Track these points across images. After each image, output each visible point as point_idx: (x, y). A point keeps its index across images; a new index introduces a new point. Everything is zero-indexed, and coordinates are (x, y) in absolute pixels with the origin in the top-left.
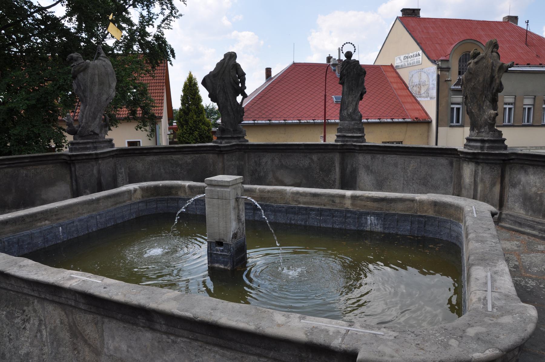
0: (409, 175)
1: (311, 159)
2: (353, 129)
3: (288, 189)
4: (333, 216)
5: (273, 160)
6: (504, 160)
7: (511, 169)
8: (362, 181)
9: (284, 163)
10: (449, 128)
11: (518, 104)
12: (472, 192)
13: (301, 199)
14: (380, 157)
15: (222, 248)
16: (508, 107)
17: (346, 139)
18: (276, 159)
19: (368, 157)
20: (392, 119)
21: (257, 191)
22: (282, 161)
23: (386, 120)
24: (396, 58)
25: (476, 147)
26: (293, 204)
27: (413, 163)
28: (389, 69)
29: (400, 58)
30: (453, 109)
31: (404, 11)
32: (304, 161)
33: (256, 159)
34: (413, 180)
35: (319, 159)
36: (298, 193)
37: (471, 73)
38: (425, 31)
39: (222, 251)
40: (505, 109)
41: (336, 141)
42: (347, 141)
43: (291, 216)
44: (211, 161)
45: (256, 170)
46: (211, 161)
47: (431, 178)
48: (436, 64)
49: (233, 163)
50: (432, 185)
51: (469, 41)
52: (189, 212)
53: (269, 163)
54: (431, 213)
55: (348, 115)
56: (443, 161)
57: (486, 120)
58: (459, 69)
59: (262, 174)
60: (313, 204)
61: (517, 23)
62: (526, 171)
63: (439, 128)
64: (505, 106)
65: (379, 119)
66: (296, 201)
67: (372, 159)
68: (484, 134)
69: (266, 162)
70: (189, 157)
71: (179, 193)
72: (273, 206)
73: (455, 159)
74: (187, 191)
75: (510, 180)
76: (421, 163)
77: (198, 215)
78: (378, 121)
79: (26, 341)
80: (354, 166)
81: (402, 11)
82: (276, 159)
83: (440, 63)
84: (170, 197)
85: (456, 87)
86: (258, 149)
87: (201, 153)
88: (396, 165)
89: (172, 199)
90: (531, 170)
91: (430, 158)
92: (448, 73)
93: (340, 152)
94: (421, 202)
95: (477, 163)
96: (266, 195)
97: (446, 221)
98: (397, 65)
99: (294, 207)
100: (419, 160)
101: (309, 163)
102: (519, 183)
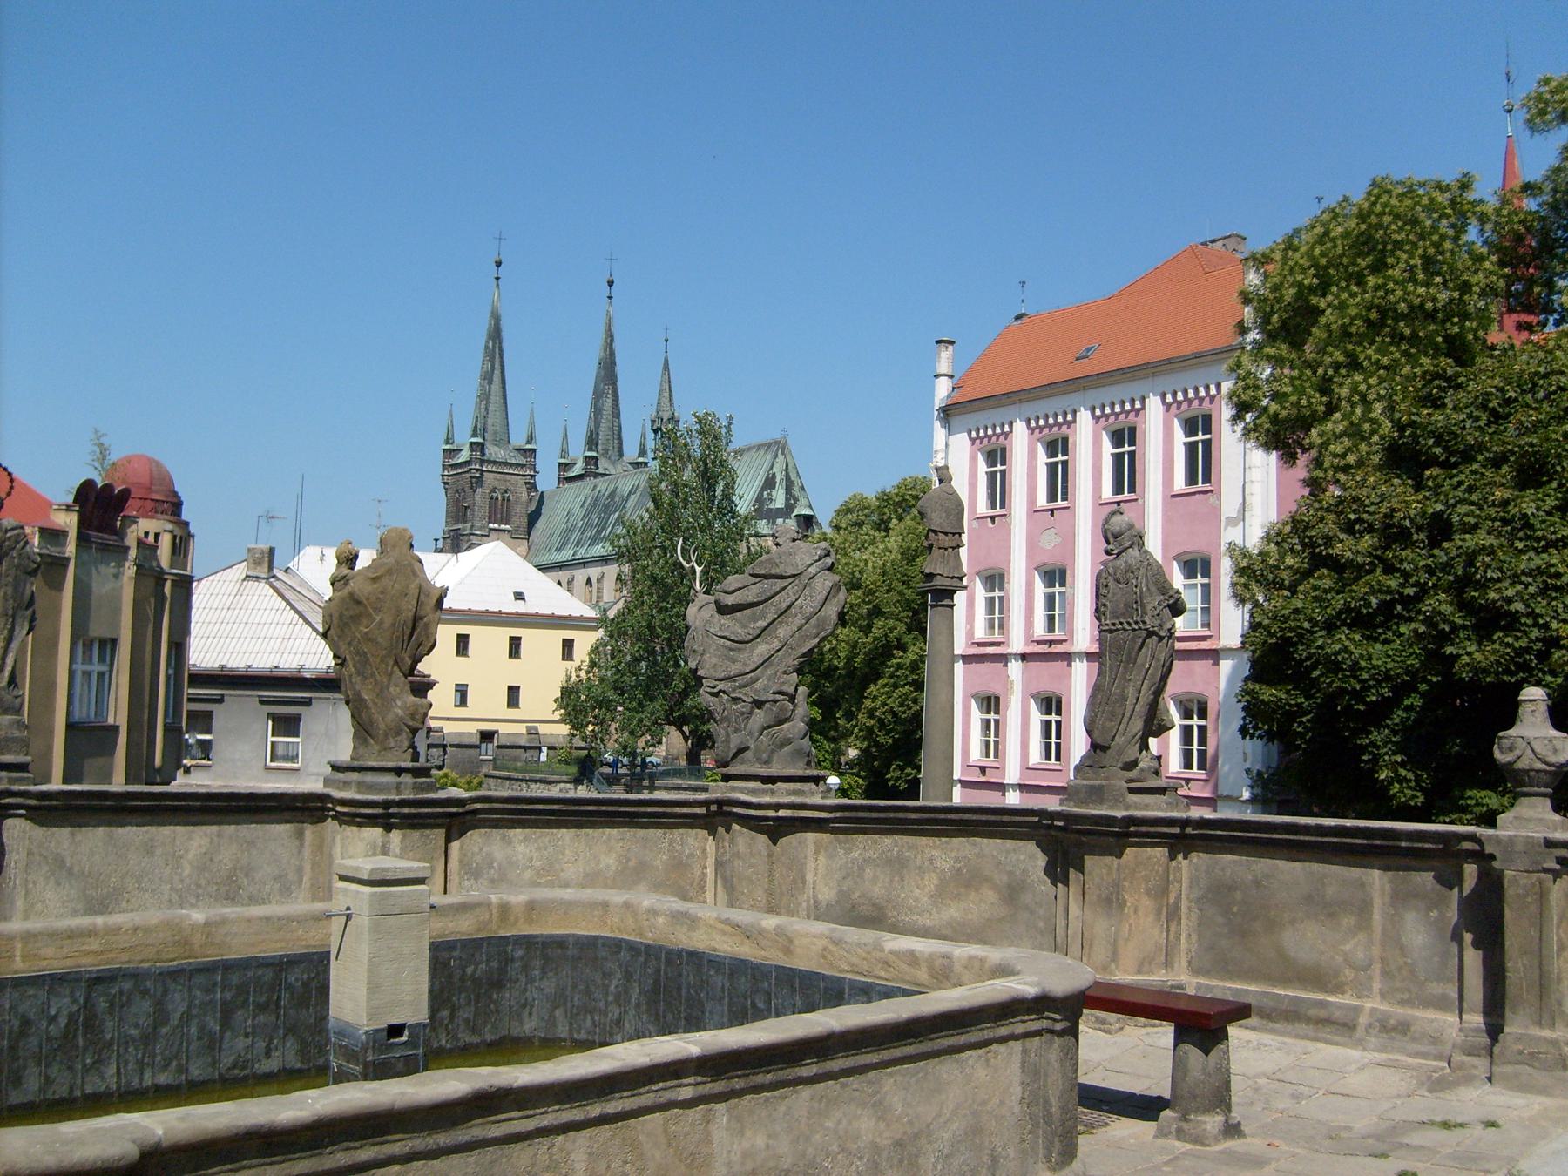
34: (199, 886)
37: (359, 602)
57: (402, 719)
88: (149, 849)
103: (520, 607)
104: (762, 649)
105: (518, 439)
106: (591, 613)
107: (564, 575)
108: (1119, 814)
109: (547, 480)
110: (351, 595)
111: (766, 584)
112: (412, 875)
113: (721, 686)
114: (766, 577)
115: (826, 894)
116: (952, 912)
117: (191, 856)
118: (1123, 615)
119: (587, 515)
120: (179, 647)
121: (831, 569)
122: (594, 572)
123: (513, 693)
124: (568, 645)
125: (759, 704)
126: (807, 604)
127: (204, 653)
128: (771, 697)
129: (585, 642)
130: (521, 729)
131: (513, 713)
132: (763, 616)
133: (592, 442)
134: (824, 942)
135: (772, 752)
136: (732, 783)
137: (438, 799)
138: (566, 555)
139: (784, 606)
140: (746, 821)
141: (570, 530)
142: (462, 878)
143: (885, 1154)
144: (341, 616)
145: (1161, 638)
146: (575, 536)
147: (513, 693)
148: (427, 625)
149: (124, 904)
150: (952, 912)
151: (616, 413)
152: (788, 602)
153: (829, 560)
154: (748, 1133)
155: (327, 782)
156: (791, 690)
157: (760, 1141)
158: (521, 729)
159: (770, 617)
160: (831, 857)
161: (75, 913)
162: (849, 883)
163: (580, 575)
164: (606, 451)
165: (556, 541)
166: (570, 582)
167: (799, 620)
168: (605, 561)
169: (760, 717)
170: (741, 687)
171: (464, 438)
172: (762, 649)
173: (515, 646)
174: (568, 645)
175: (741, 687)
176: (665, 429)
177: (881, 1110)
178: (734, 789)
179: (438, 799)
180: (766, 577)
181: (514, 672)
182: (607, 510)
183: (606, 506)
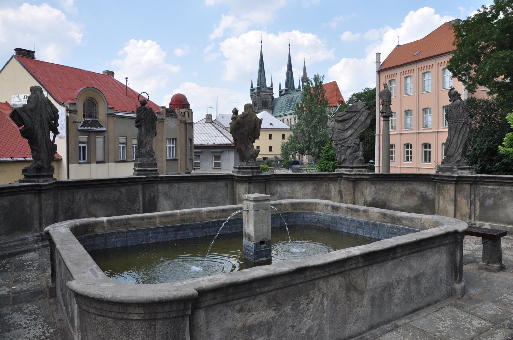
0: (198, 196)
1: (120, 192)
2: (152, 164)
3: (204, 209)
4: (236, 224)
5: (86, 196)
6: (266, 179)
7: (269, 184)
8: (162, 206)
9: (96, 198)
10: (78, 165)
11: (129, 144)
13: (214, 215)
14: (176, 185)
15: (265, 245)
16: (121, 145)
17: (147, 172)
18: (89, 194)
19: (167, 186)
20: (24, 158)
21: (179, 214)
22: (95, 196)
23: (18, 159)
24: (13, 96)
25: (249, 173)
26: (208, 220)
27: (201, 187)
28: (5, 107)
29: (18, 97)
30: (80, 147)
31: (18, 50)
32: (114, 194)
33: (69, 196)
35: (126, 192)
36: (211, 211)
37: (239, 124)
38: (45, 74)
39: (265, 247)
40: (80, 147)
41: (134, 174)
42: (148, 174)
43: (207, 230)
44: (28, 202)
45: (70, 207)
46: (28, 202)
48: (64, 106)
49: (50, 202)
50: (215, 203)
51: (91, 88)
52: (108, 247)
53: (83, 198)
54: (290, 210)
55: (147, 152)
56: (221, 184)
57: (252, 155)
58: (84, 112)
59: (76, 210)
60: (223, 218)
61: (114, 77)
62: (280, 185)
63: (70, 165)
64: (80, 145)
65: (11, 158)
66: (210, 218)
67: (169, 187)
68: (251, 164)
69: (80, 198)
70: (6, 199)
71: (96, 230)
72: (192, 225)
73: (229, 182)
74: (106, 226)
76: (206, 187)
77: (119, 247)
78: (10, 159)
80: (152, 195)
81: (15, 50)
82: (89, 194)
83: (68, 105)
84: (86, 235)
85: (83, 128)
86: (182, 180)
87: (20, 194)
88: (188, 190)
89: (88, 237)
90: (284, 184)
91: (213, 183)
92: (75, 115)
93: (142, 184)
94: (285, 205)
95: (250, 183)
96: (187, 217)
97: (300, 213)
98: (15, 103)
99: (209, 223)
100: (205, 185)
101: (119, 196)
102: (277, 192)
103: (272, 127)
104: (350, 132)
105: (268, 85)
106: (289, 127)
108: (456, 175)
109: (276, 95)
110: (237, 122)
111: (349, 114)
112: (265, 199)
113: (338, 142)
114: (350, 112)
115: (369, 199)
118: (456, 118)
119: (287, 103)
120: (191, 140)
121: (368, 109)
122: (289, 117)
123: (271, 149)
124: (283, 136)
125: (349, 147)
126: (362, 119)
127: (197, 141)
128: (352, 145)
129: (288, 135)
130: (273, 157)
131: (271, 153)
132: (349, 123)
135: (353, 160)
137: (259, 177)
138: (282, 114)
139: (355, 120)
140: (346, 179)
141: (282, 107)
143: (412, 280)
145: (468, 125)
146: (284, 109)
147: (271, 149)
148: (257, 129)
153: (367, 107)
154: (374, 276)
155: (233, 172)
156: (358, 143)
157: (378, 279)
158: (273, 157)
159: (351, 123)
160: (371, 188)
162: (376, 195)
163: (286, 118)
165: (279, 111)
166: (283, 120)
167: (359, 124)
168: (291, 114)
169: (349, 151)
171: (255, 86)
172: (350, 132)
173: (270, 137)
174: (283, 136)
176: (305, 79)
177: (411, 268)
178: (342, 170)
179: (259, 177)
180: (350, 112)
181: (271, 143)
182: (291, 102)
183: (290, 101)
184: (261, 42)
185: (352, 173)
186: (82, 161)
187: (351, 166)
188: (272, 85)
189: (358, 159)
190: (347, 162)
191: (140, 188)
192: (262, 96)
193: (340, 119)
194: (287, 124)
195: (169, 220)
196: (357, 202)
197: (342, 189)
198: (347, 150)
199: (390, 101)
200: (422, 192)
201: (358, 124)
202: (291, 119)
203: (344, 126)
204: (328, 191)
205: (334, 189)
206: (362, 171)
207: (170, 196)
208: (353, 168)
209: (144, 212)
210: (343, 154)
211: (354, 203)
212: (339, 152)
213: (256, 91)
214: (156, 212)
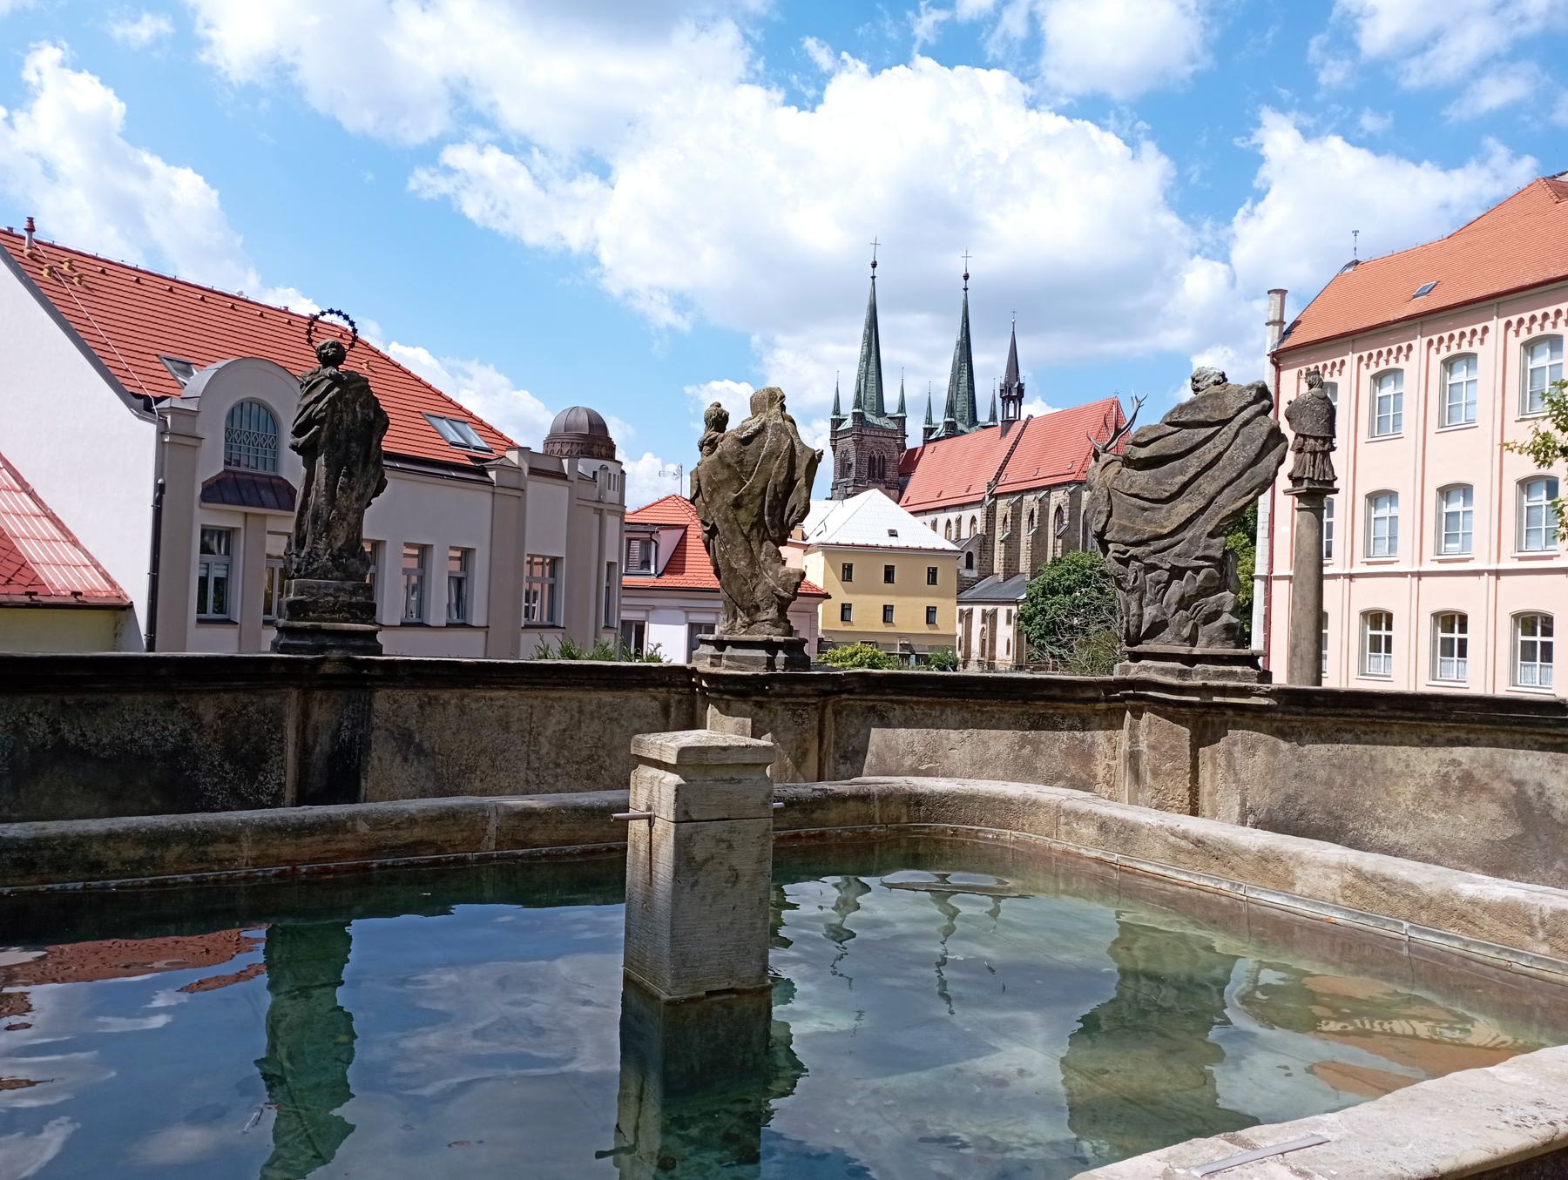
0: (544, 751)
1: (194, 716)
12: (1182, 791)
18: (35, 719)
19: (409, 699)
22: (65, 727)
34: (558, 765)
47: (609, 755)
75: (836, 743)
79: (493, 208)
101: (184, 732)
103: (894, 542)
104: (1183, 508)
105: (891, 407)
107: (929, 518)
109: (914, 439)
113: (1133, 551)
115: (1263, 799)
116: (1440, 825)
117: (549, 733)
122: (953, 516)
132: (1182, 472)
133: (950, 410)
134: (1349, 877)
136: (1143, 662)
139: (1209, 457)
140: (1161, 707)
142: (836, 762)
144: (710, 482)
149: (477, 784)
150: (1440, 825)
151: (971, 387)
152: (1215, 453)
159: (1192, 472)
161: (423, 794)
163: (942, 518)
164: (962, 418)
166: (934, 525)
170: (1154, 552)
171: (847, 409)
172: (1183, 508)
175: (1154, 552)
178: (1145, 668)
184: (874, 265)
185: (1188, 683)
186: (210, 615)
187: (1183, 650)
188: (902, 408)
189: (1218, 623)
190: (1167, 634)
191: (290, 704)
192: (868, 441)
193: (1143, 453)
194: (948, 537)
195: (312, 845)
196: (1204, 801)
197: (1143, 747)
198: (1168, 583)
199: (1328, 436)
200: (1519, 784)
201: (1221, 474)
202: (959, 521)
203: (1159, 483)
204: (1087, 757)
205: (1108, 746)
206: (1232, 675)
207: (419, 745)
208: (1191, 660)
209: (299, 801)
210: (1153, 602)
211: (1194, 812)
212: (1133, 590)
213: (848, 424)
214: (354, 800)
